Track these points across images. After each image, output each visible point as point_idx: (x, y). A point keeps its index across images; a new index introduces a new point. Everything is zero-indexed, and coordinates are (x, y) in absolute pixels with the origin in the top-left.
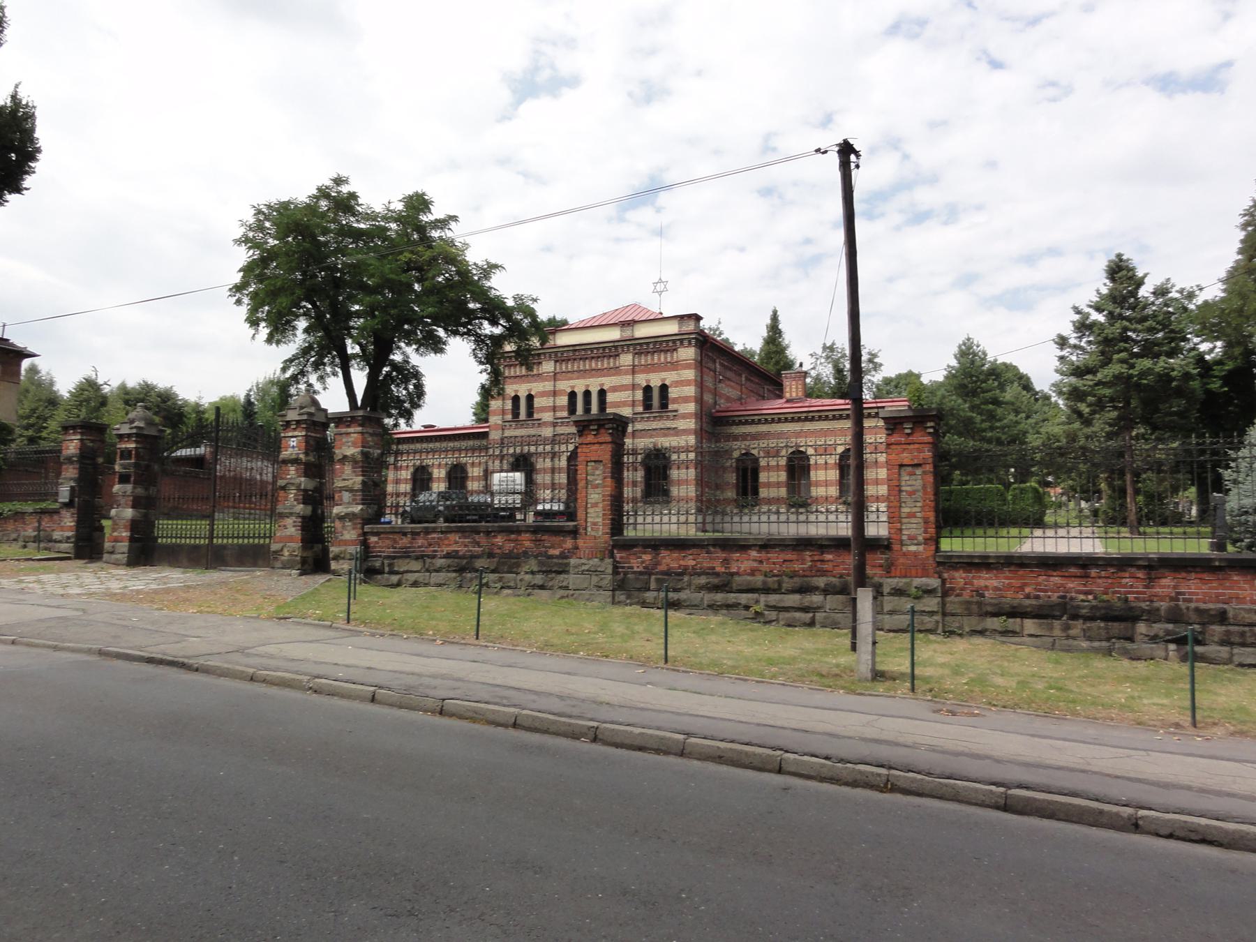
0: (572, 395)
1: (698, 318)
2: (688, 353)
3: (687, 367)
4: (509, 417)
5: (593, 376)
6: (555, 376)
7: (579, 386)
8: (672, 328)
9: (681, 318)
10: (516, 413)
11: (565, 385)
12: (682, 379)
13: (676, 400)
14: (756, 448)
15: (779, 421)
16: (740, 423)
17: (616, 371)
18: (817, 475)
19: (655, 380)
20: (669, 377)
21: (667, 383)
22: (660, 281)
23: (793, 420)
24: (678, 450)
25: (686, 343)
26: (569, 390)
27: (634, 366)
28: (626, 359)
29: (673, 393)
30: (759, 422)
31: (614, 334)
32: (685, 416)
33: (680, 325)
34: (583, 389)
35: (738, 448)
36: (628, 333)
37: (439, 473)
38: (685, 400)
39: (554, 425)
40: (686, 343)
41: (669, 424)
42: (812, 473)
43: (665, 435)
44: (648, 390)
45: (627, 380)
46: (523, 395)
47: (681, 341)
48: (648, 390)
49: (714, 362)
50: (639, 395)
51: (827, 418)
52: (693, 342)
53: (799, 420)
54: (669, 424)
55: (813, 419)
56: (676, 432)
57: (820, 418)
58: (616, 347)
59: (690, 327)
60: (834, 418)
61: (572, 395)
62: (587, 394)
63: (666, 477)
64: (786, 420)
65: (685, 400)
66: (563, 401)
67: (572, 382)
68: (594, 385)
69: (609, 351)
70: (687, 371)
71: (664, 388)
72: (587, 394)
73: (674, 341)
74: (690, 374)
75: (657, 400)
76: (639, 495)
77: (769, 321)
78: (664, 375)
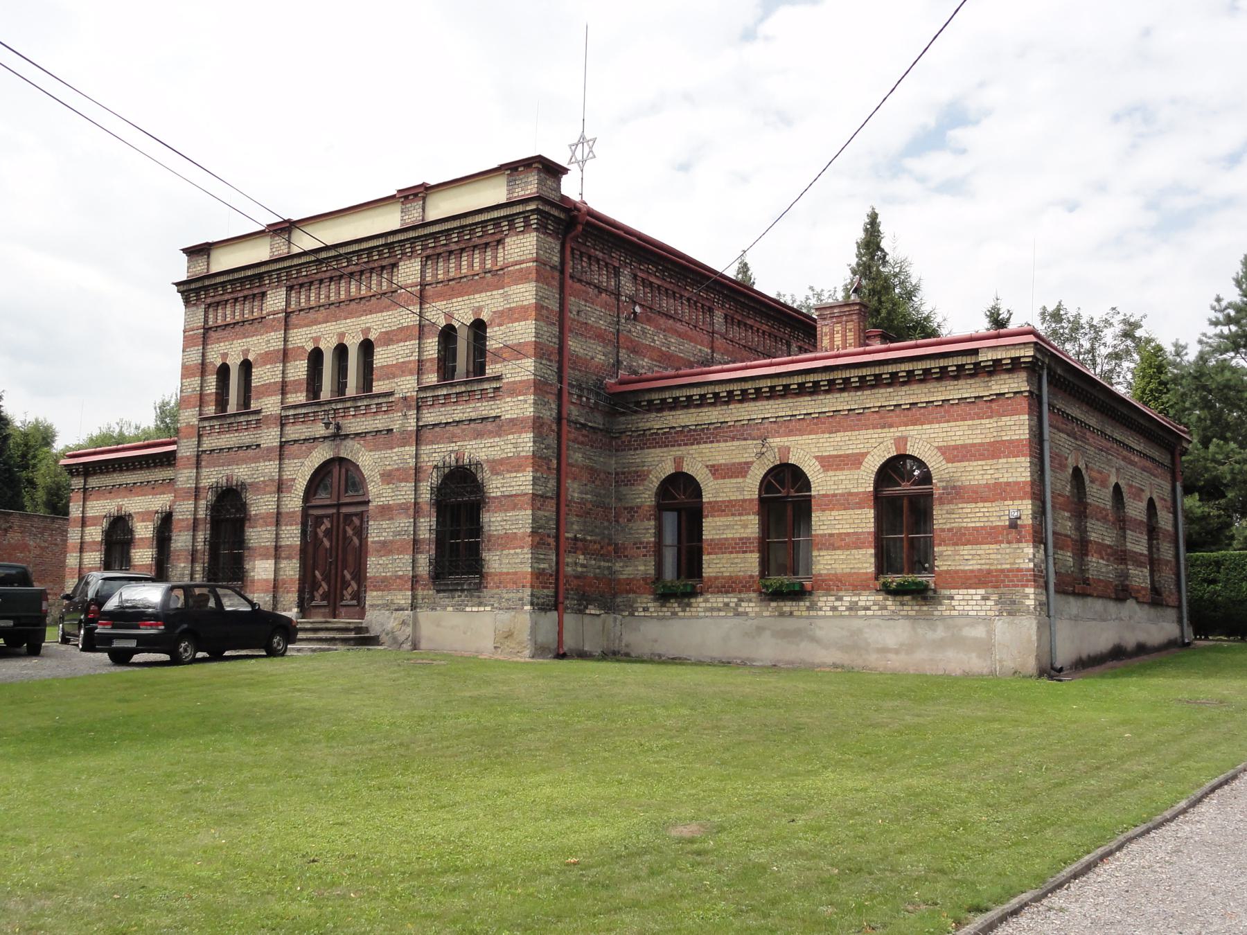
0: (316, 357)
1: (551, 170)
2: (522, 247)
3: (522, 277)
4: (210, 410)
5: (350, 315)
6: (287, 320)
7: (327, 335)
8: (494, 194)
9: (513, 169)
10: (222, 401)
11: (302, 338)
12: (508, 303)
13: (498, 356)
14: (697, 461)
15: (744, 397)
16: (664, 406)
17: (390, 298)
18: (824, 522)
19: (462, 312)
20: (488, 303)
21: (485, 317)
22: (582, 140)
23: (773, 394)
24: (498, 466)
25: (519, 223)
26: (310, 347)
27: (423, 285)
28: (409, 272)
29: (496, 338)
30: (702, 402)
31: (390, 220)
32: (515, 390)
33: (511, 184)
34: (334, 342)
35: (661, 464)
36: (414, 216)
37: (144, 530)
38: (516, 352)
39: (282, 422)
40: (519, 223)
41: (484, 408)
42: (815, 516)
43: (479, 435)
44: (448, 335)
45: (406, 317)
46: (234, 362)
47: (510, 219)
48: (448, 335)
49: (617, 273)
50: (432, 347)
51: (846, 386)
52: (534, 219)
53: (786, 392)
54: (484, 408)
55: (815, 389)
56: (495, 425)
57: (832, 387)
58: (390, 246)
59: (530, 186)
60: (863, 384)
61: (316, 357)
62: (341, 351)
63: (476, 529)
64: (759, 395)
65: (516, 352)
66: (299, 370)
67: (315, 330)
68: (351, 330)
69: (376, 256)
70: (522, 288)
71: (479, 327)
72: (341, 351)
73: (496, 222)
74: (525, 293)
75: (462, 357)
76: (424, 568)
77: (860, 235)
78: (480, 299)
